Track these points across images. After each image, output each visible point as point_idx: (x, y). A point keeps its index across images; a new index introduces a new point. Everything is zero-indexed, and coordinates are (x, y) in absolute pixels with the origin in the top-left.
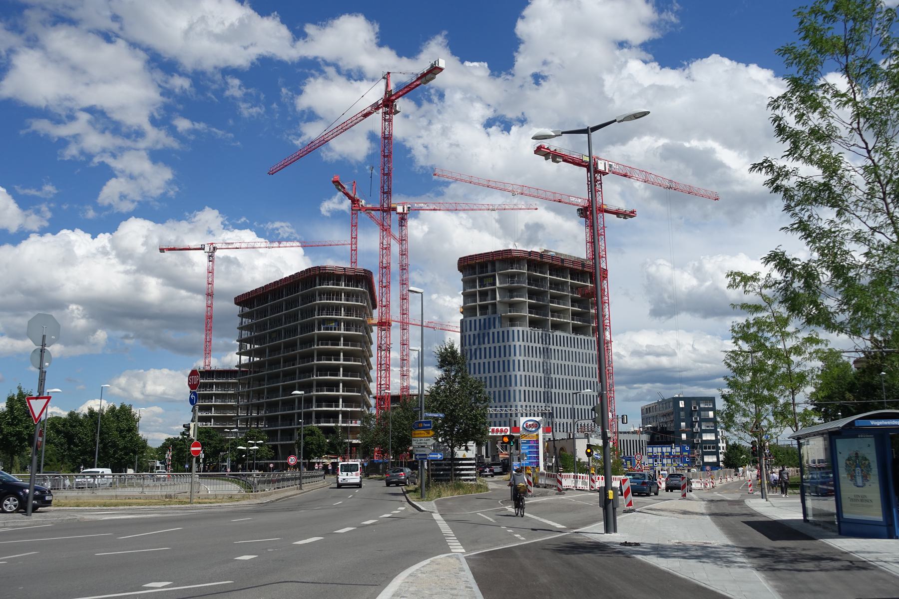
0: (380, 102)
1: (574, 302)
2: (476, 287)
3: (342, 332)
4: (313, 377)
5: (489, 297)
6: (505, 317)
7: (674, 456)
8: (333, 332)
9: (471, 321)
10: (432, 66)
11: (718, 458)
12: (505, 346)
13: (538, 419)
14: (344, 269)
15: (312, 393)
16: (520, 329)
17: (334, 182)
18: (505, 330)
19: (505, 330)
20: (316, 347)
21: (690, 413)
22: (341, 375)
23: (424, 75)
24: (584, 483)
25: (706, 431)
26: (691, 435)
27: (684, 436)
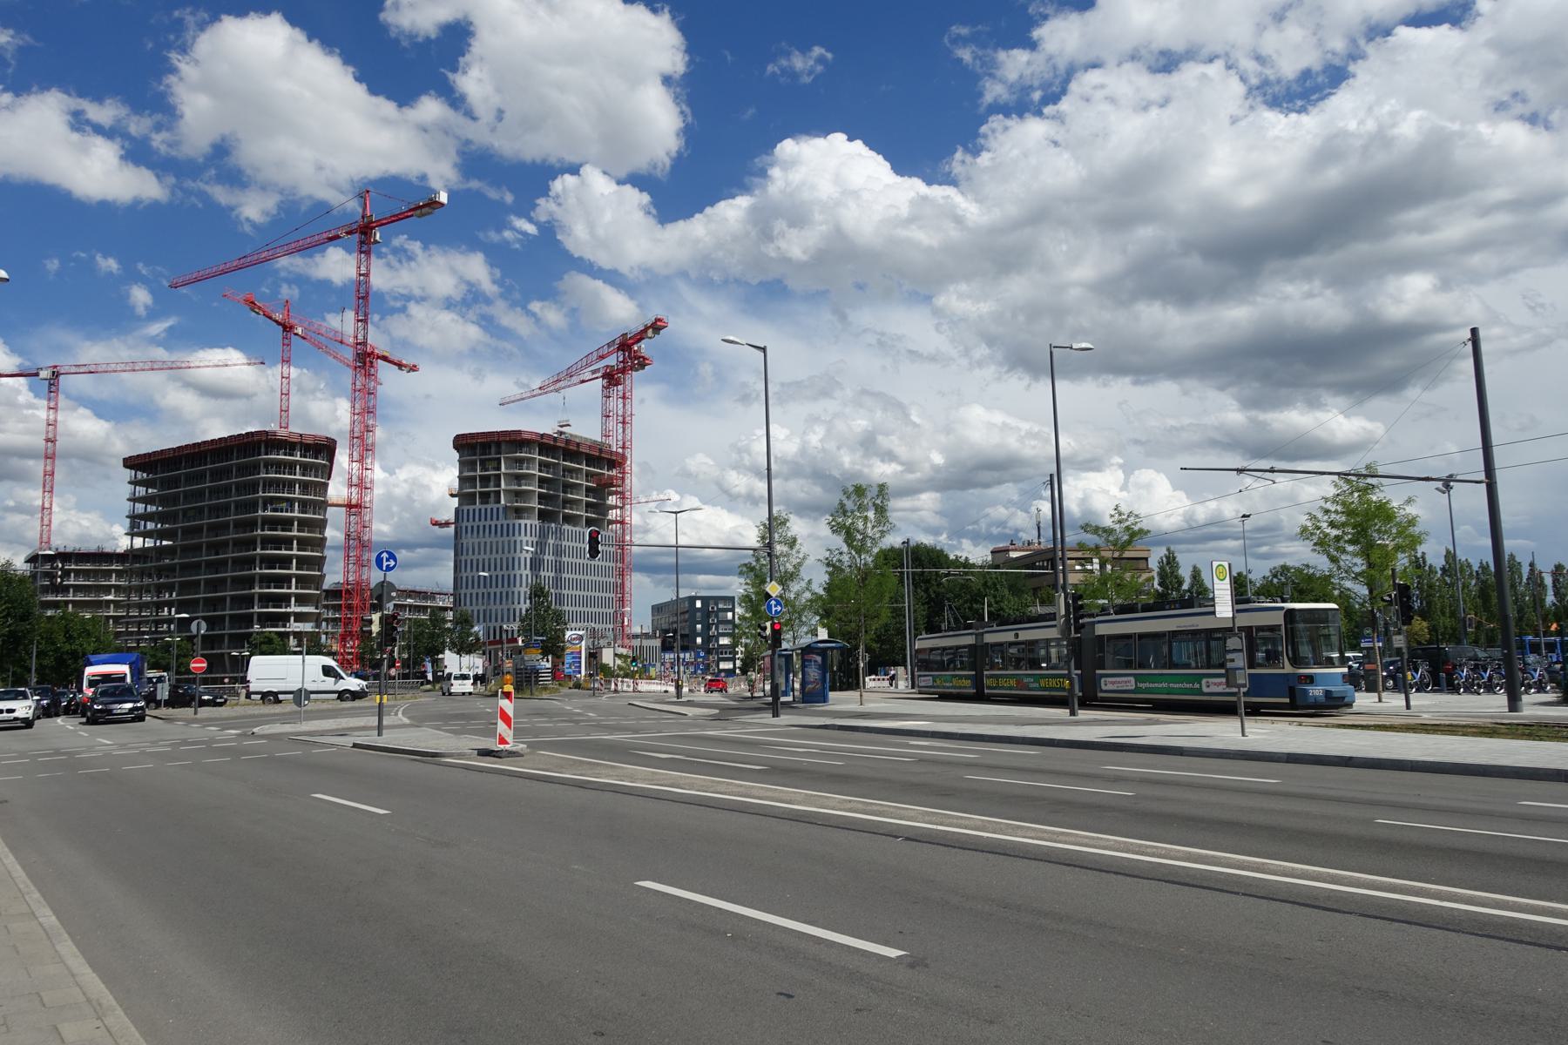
3: (296, 514)
4: (255, 569)
5: (492, 483)
7: (687, 663)
8: (284, 514)
9: (468, 510)
11: (734, 664)
13: (581, 633)
14: (301, 435)
15: (253, 591)
16: (528, 522)
20: (259, 532)
21: (706, 613)
22: (294, 568)
24: (628, 686)
25: (724, 635)
26: (708, 639)
27: (699, 640)
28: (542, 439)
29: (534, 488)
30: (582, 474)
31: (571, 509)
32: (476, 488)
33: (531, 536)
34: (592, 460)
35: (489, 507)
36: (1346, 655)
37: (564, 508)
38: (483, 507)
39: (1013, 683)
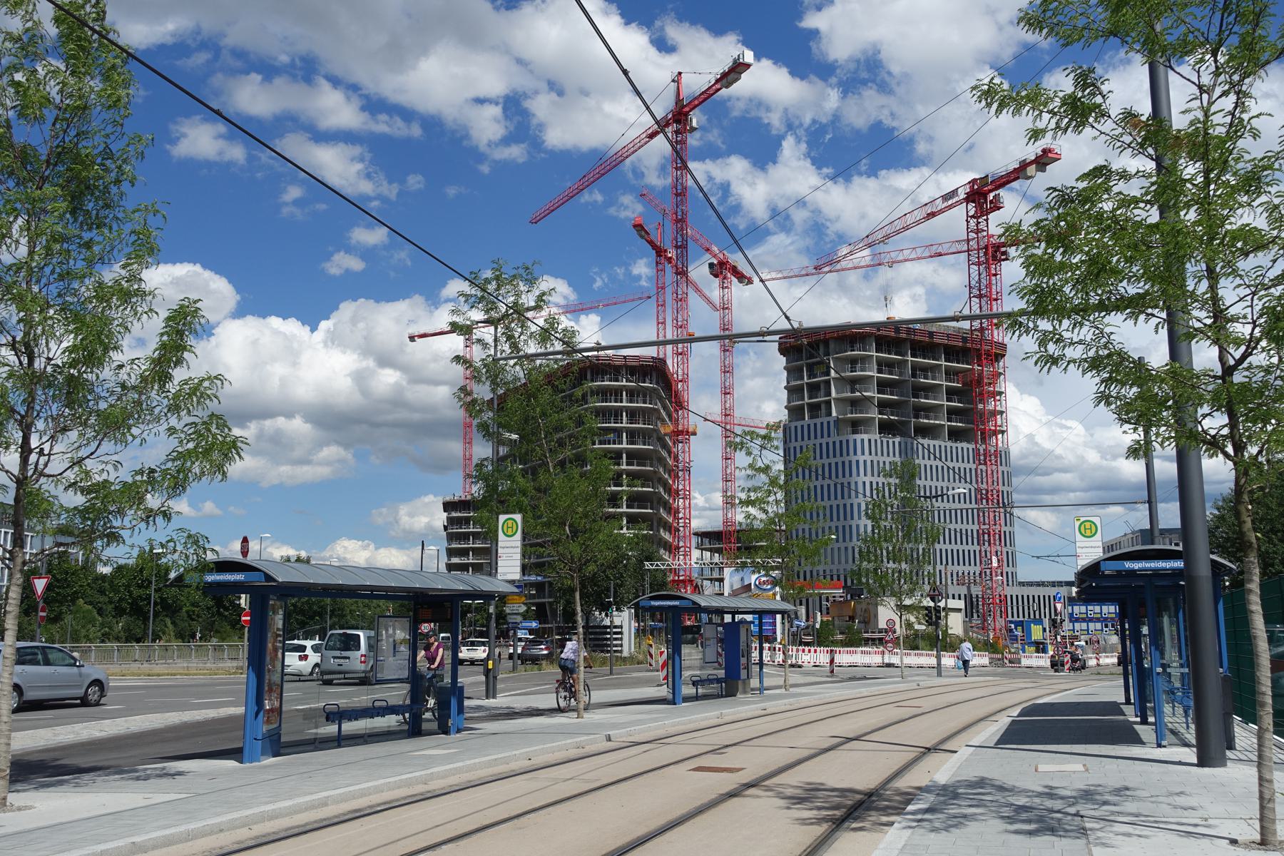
0: (670, 116)
1: (951, 393)
2: (803, 379)
3: (624, 446)
5: (822, 392)
6: (845, 420)
7: (1106, 619)
8: (612, 446)
9: (796, 427)
10: (735, 61)
12: (843, 463)
16: (866, 437)
17: (635, 226)
18: (844, 438)
19: (844, 438)
23: (724, 75)
28: (879, 330)
29: (872, 393)
30: (940, 371)
31: (927, 418)
32: (803, 399)
33: (870, 454)
34: (952, 353)
35: (818, 421)
36: (243, 596)
37: (917, 417)
38: (812, 422)
39: (915, 684)
